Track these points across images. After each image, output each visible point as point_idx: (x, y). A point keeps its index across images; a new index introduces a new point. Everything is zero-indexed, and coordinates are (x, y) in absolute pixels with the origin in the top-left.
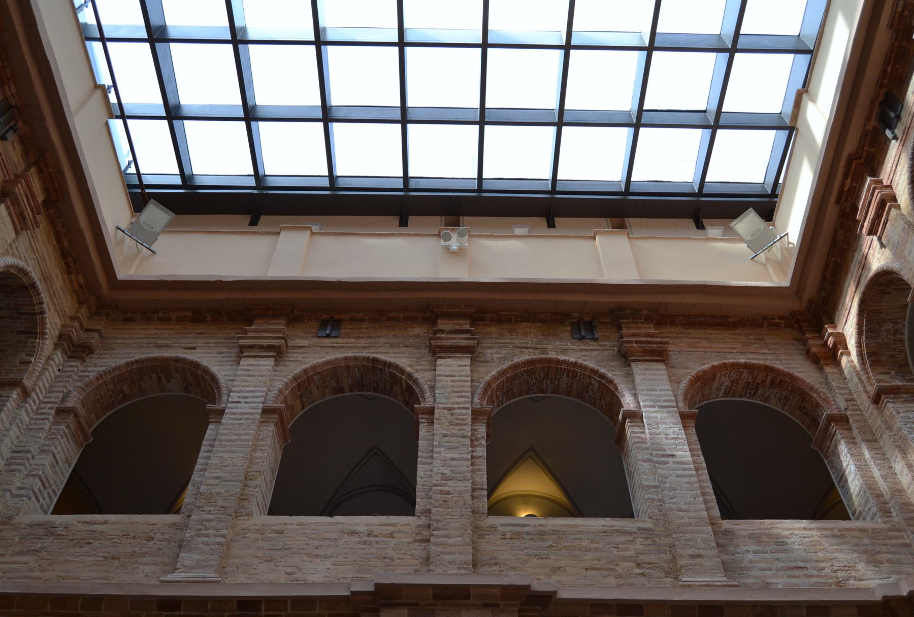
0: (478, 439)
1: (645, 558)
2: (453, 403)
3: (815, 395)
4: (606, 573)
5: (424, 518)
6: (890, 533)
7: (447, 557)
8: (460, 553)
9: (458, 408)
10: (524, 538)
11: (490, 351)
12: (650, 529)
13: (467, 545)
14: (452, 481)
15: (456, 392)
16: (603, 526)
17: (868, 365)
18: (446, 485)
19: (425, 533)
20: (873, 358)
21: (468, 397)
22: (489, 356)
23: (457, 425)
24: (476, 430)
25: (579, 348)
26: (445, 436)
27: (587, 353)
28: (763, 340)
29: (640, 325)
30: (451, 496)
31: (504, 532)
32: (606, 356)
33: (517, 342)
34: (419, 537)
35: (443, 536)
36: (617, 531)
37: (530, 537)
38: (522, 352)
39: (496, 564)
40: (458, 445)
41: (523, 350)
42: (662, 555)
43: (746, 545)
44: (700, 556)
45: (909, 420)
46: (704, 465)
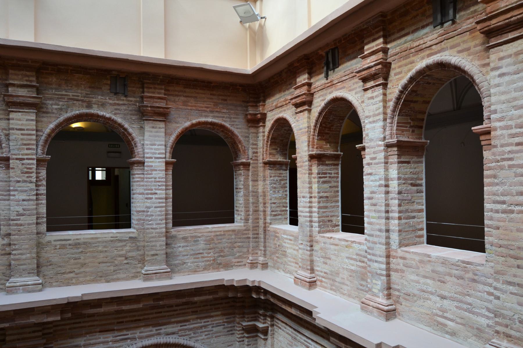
0: (41, 180)
1: (130, 254)
2: (22, 155)
3: (240, 146)
4: (109, 264)
5: (6, 239)
6: (244, 232)
7: (21, 267)
8: (29, 264)
9: (28, 159)
10: (67, 248)
11: (50, 102)
12: (135, 238)
13: (33, 259)
14: (24, 217)
15: (25, 145)
16: (112, 237)
17: (269, 143)
18: (19, 220)
19: (7, 249)
20: (273, 140)
21: (33, 149)
22: (49, 106)
23: (27, 173)
24: (39, 173)
25: (113, 102)
26: (18, 182)
27: (118, 107)
28: (226, 100)
29: (156, 86)
30: (23, 227)
31: (56, 245)
32: (131, 111)
33: (71, 94)
34: (3, 252)
35: (19, 254)
36: (118, 240)
37: (71, 247)
38: (74, 104)
39: (50, 265)
40: (26, 189)
41: (75, 102)
42: (139, 252)
43: (180, 243)
44: (157, 255)
45: (273, 182)
46: (171, 196)
